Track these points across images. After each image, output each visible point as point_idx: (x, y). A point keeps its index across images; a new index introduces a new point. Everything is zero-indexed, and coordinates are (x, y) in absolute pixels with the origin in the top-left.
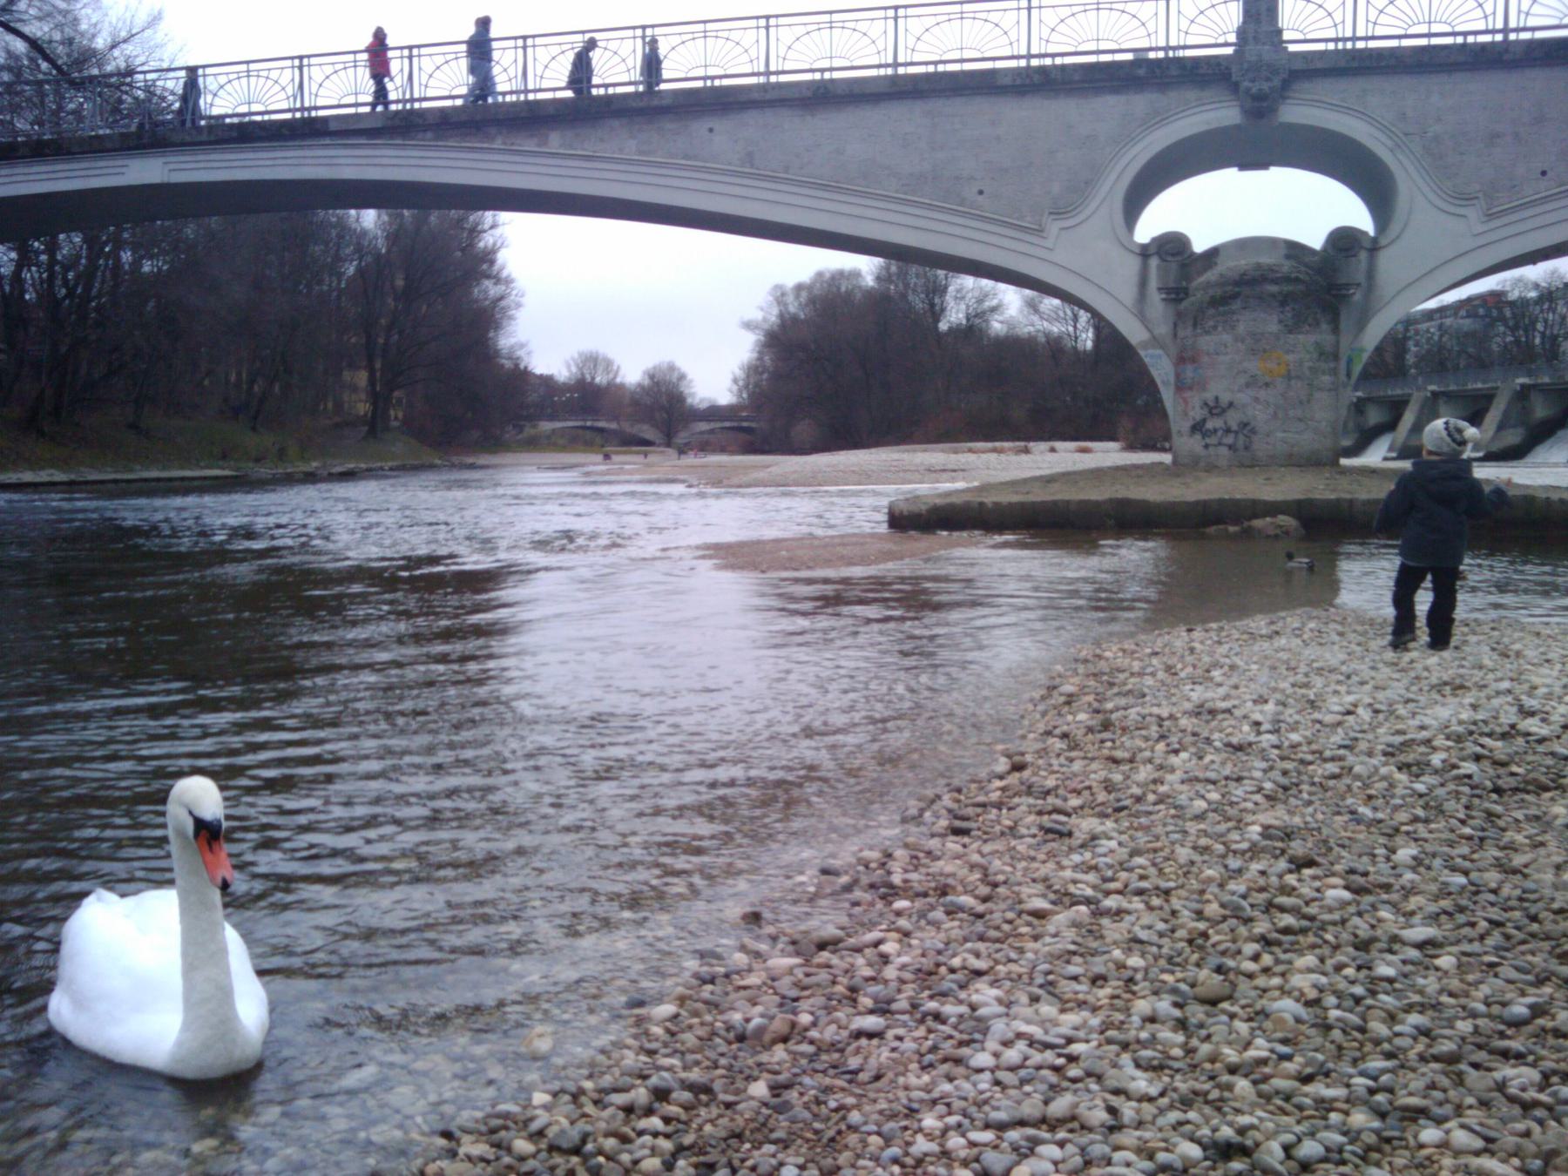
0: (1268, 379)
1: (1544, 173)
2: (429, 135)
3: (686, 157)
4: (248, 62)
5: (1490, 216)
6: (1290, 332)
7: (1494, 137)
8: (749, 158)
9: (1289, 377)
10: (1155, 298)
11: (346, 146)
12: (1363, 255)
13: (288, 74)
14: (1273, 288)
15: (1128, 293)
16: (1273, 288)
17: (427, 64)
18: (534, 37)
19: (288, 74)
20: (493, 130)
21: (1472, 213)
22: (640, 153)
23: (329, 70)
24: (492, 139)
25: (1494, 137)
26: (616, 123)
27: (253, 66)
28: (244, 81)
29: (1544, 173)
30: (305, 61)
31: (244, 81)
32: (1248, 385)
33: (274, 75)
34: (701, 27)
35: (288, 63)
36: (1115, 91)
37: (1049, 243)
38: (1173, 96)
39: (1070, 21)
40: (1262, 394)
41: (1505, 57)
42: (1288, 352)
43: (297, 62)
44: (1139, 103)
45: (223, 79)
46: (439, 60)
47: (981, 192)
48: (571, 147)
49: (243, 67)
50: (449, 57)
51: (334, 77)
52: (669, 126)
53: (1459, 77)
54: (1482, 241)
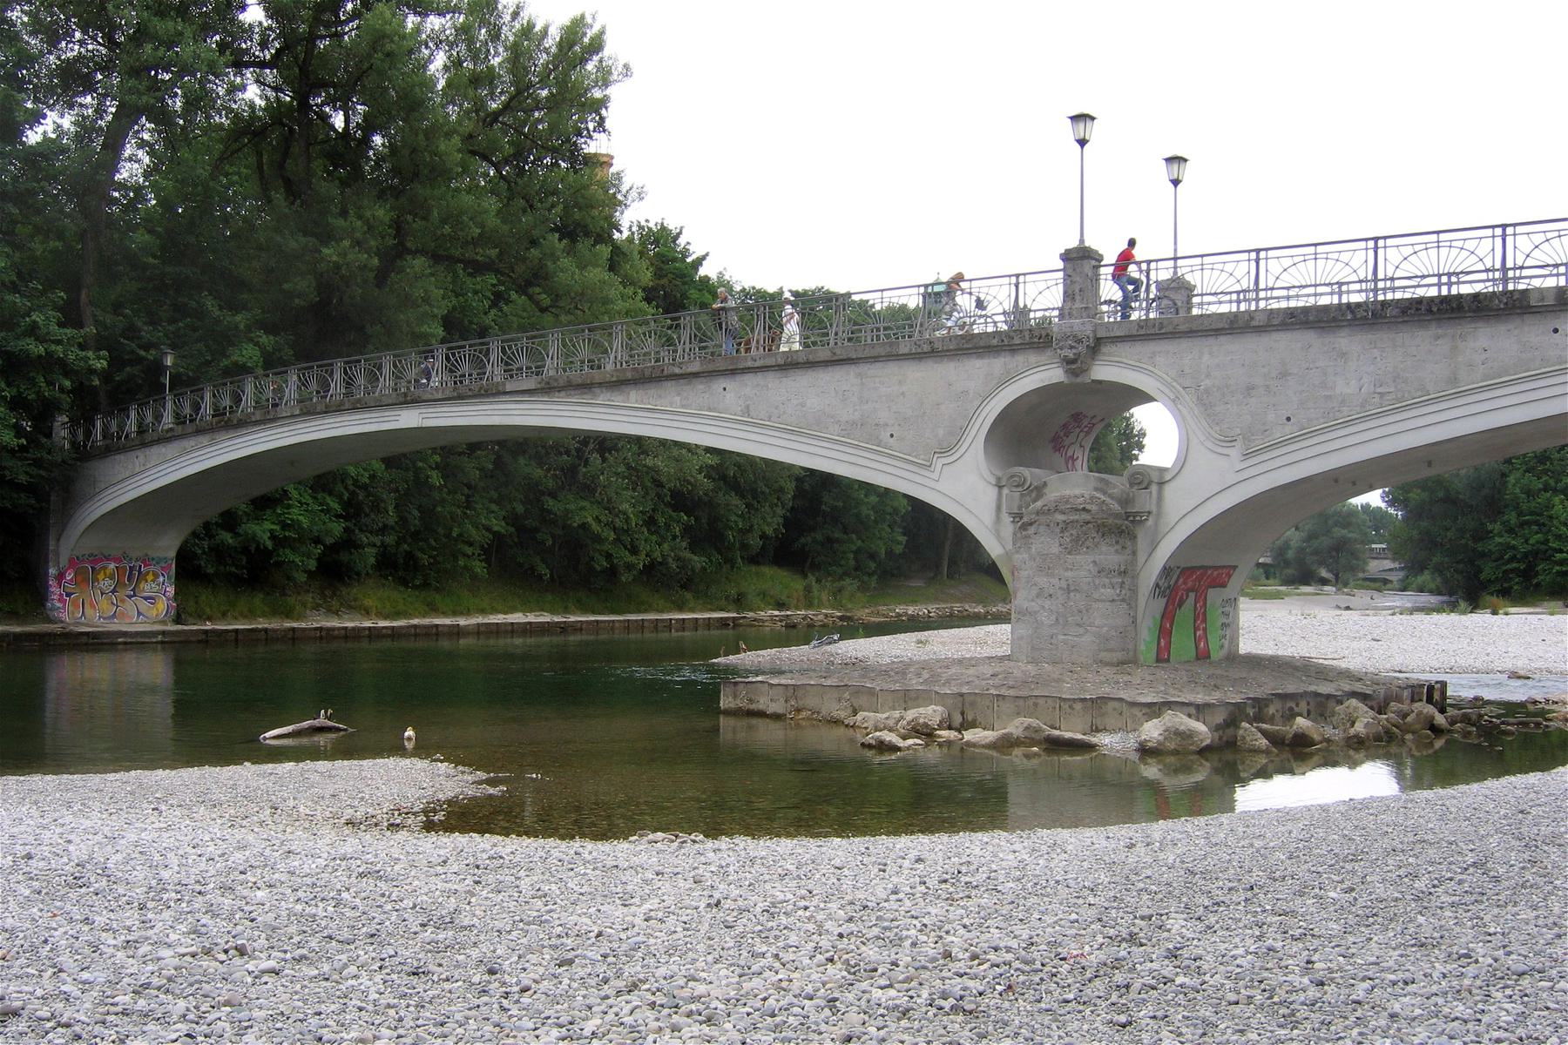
0: (1051, 591)
1: (1288, 419)
2: (563, 394)
3: (710, 410)
4: (1438, 232)
5: (1247, 456)
6: (1069, 553)
7: (1250, 389)
8: (747, 411)
9: (1068, 590)
10: (1007, 519)
11: (491, 403)
12: (1154, 488)
13: (1244, 267)
14: (1060, 517)
15: (988, 516)
16: (1060, 517)
17: (1275, 267)
18: (1267, 250)
19: (1244, 267)
20: (597, 390)
21: (1235, 453)
22: (683, 406)
23: (1042, 286)
24: (595, 396)
25: (1250, 389)
26: (669, 384)
27: (1443, 237)
28: (1433, 252)
29: (1288, 419)
30: (1021, 279)
31: (1433, 252)
32: (1038, 596)
33: (1345, 257)
34: (1312, 249)
35: (1245, 256)
36: (980, 355)
37: (935, 476)
38: (1020, 359)
39: (1413, 258)
40: (1047, 603)
41: (1254, 323)
42: (1067, 569)
43: (1014, 280)
44: (998, 364)
45: (1538, 239)
46: (1287, 262)
47: (892, 436)
48: (642, 403)
49: (1434, 237)
50: (1296, 259)
51: (1046, 293)
52: (701, 387)
53: (1222, 339)
54: (1246, 474)
